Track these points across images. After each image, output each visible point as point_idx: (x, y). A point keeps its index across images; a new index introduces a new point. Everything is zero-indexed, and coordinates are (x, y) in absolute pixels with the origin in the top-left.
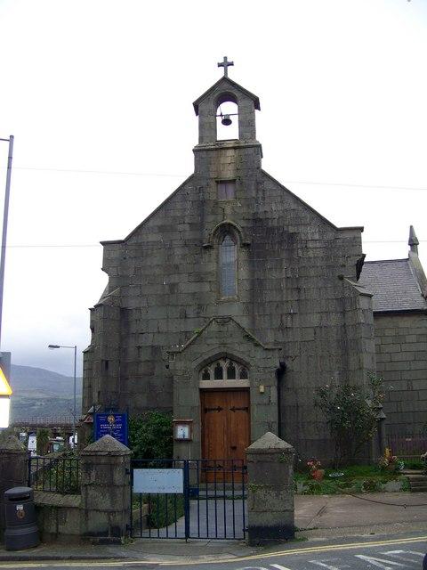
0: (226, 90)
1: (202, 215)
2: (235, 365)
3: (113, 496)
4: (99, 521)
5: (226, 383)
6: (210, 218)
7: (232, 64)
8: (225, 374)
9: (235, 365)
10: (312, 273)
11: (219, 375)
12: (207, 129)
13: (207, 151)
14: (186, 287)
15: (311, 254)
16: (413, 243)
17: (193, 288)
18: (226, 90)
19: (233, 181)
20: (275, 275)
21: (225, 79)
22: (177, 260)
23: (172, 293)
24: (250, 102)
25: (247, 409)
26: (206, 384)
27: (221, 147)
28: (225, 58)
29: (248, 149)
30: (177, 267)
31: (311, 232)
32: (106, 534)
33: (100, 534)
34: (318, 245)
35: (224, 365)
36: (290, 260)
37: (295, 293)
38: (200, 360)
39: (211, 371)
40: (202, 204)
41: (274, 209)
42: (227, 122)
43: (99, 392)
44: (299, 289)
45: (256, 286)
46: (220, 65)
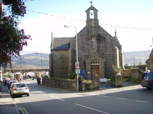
0: (92, 8)
1: (88, 33)
2: (97, 61)
3: (98, 82)
4: (96, 86)
5: (95, 64)
6: (90, 34)
7: (92, 2)
8: (95, 63)
9: (97, 61)
10: (108, 45)
11: (94, 63)
12: (88, 16)
13: (89, 21)
14: (86, 46)
15: (108, 41)
16: (115, 33)
17: (87, 47)
18: (92, 8)
19: (94, 27)
20: (102, 45)
21: (92, 6)
22: (84, 42)
23: (83, 48)
24: (96, 11)
25: (98, 69)
26: (93, 64)
27: (91, 20)
28: (91, 1)
29: (96, 20)
30: (84, 43)
31: (108, 37)
32: (97, 88)
33: (96, 88)
34: (109, 40)
35: (95, 61)
36: (104, 42)
37: (105, 48)
38: (91, 60)
39: (93, 62)
40: (88, 31)
41: (101, 33)
42: (92, 15)
43: (71, 66)
44: (106, 48)
45: (99, 47)
46: (90, 2)
